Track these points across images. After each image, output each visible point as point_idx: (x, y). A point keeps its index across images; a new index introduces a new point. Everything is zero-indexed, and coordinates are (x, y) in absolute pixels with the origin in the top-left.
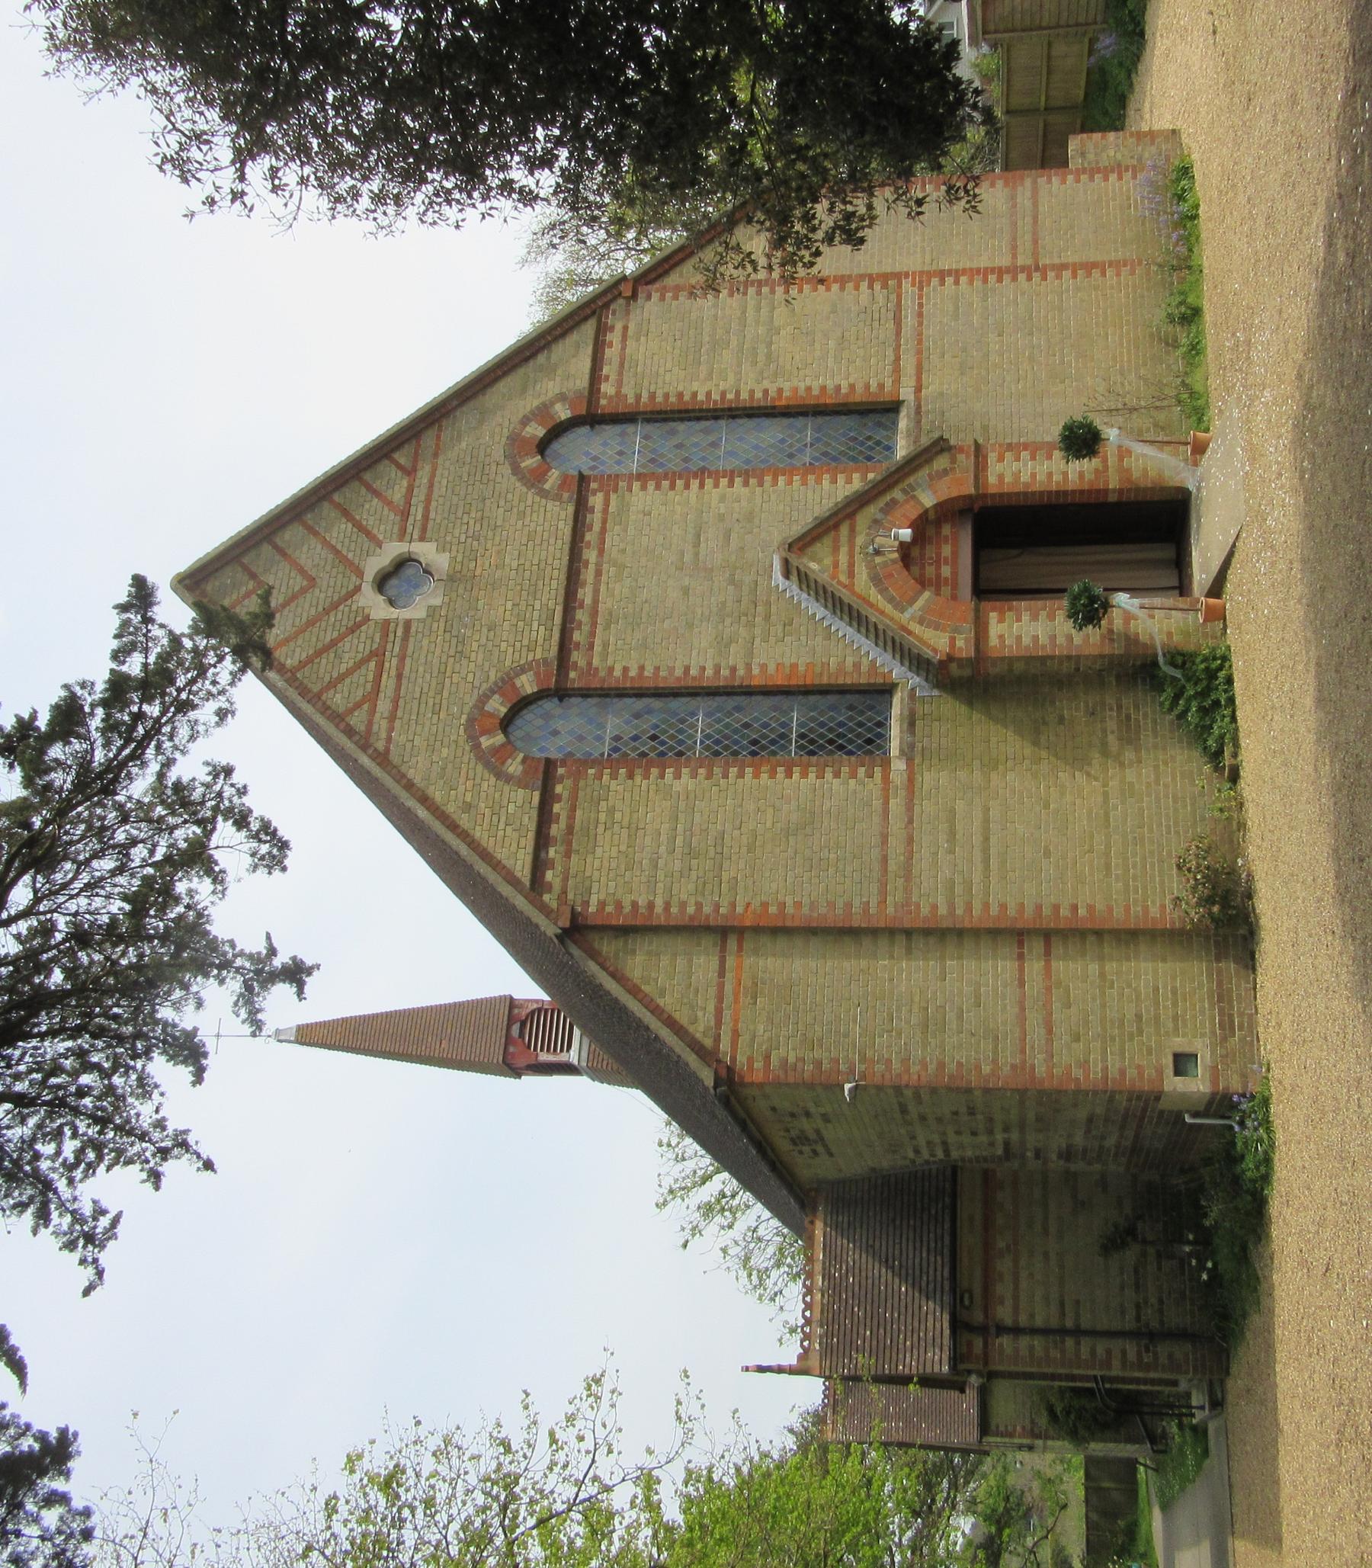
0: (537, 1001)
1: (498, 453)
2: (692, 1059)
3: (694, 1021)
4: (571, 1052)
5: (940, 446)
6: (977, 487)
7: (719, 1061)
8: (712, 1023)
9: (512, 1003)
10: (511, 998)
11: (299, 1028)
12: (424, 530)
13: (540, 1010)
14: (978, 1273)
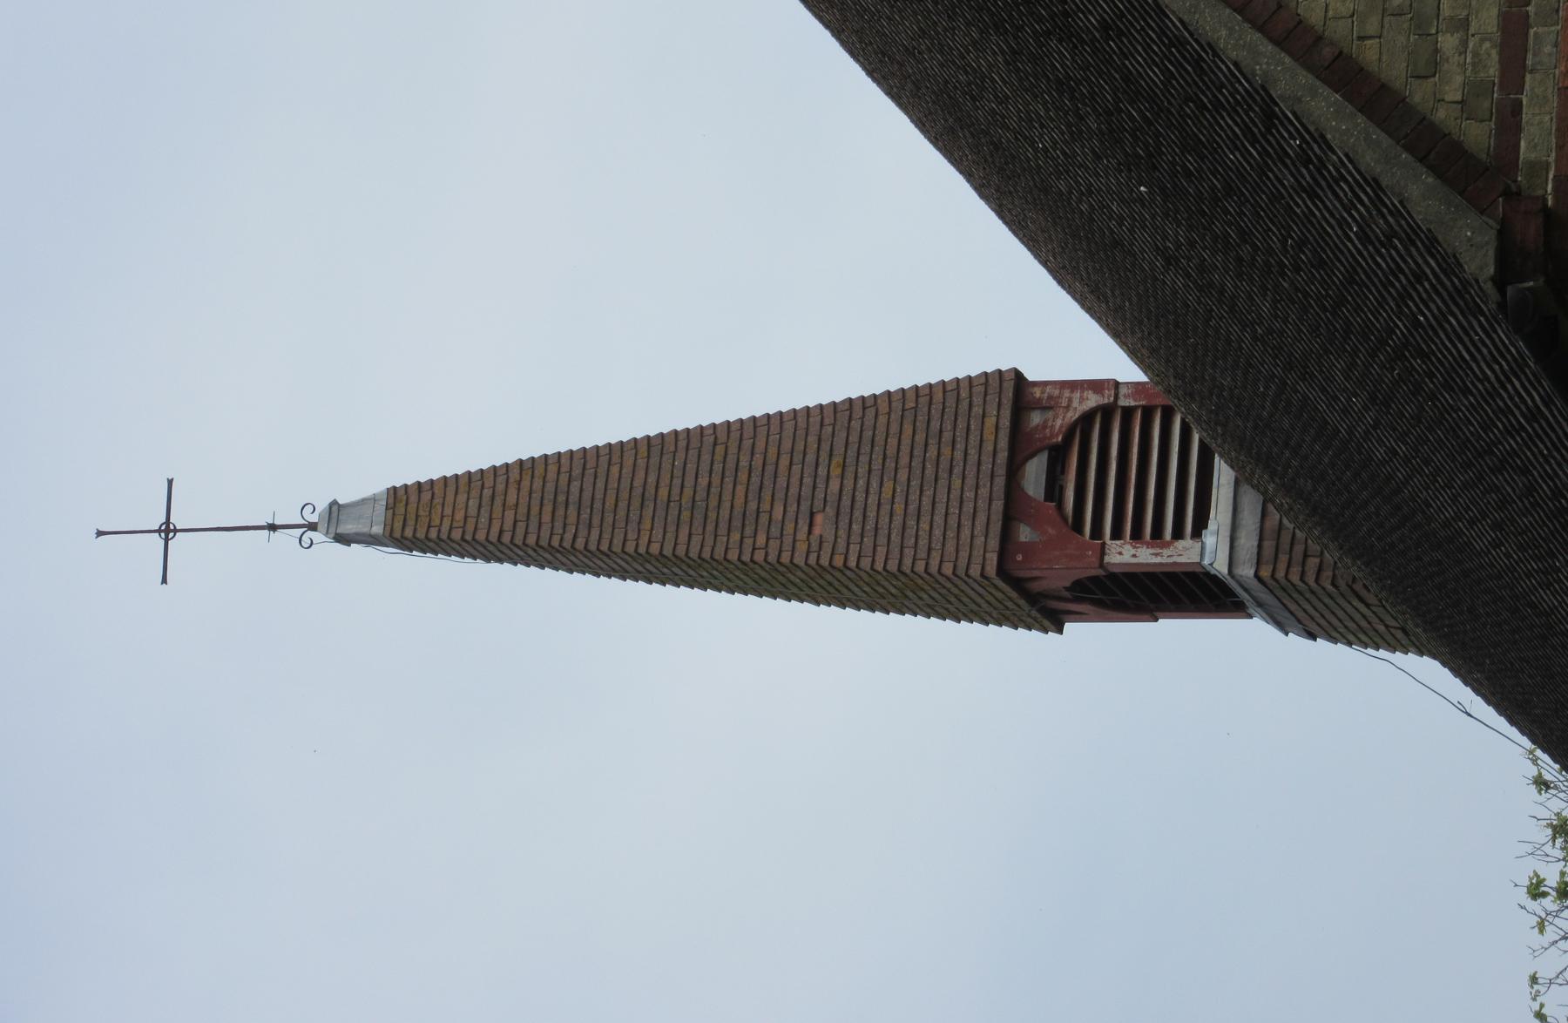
0: (1096, 386)
2: (1419, 193)
3: (1432, 66)
4: (1209, 539)
7: (1512, 195)
8: (1493, 71)
9: (1016, 391)
10: (1018, 375)
11: (396, 496)
13: (1105, 411)
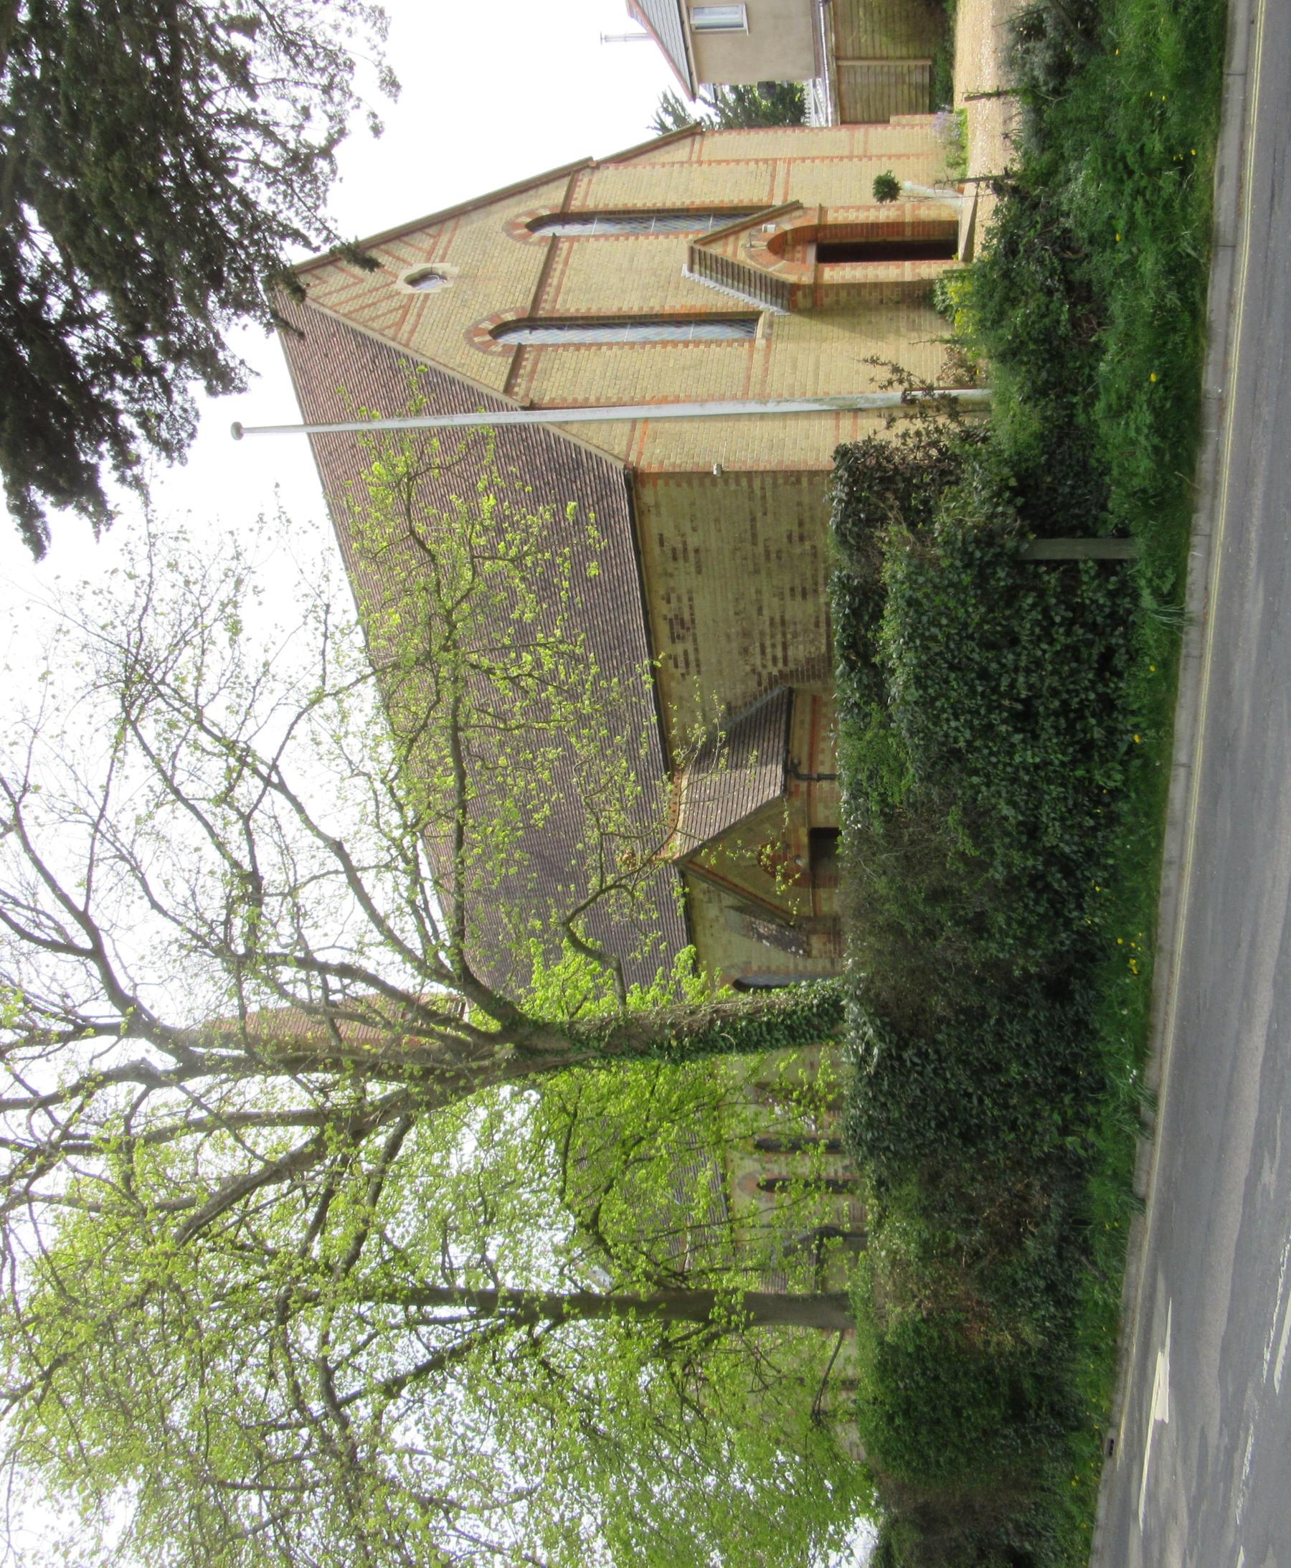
1: (498, 228)
5: (796, 206)
6: (816, 278)
12: (445, 254)
14: (806, 748)
